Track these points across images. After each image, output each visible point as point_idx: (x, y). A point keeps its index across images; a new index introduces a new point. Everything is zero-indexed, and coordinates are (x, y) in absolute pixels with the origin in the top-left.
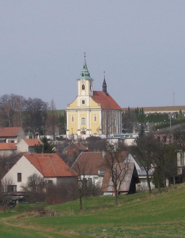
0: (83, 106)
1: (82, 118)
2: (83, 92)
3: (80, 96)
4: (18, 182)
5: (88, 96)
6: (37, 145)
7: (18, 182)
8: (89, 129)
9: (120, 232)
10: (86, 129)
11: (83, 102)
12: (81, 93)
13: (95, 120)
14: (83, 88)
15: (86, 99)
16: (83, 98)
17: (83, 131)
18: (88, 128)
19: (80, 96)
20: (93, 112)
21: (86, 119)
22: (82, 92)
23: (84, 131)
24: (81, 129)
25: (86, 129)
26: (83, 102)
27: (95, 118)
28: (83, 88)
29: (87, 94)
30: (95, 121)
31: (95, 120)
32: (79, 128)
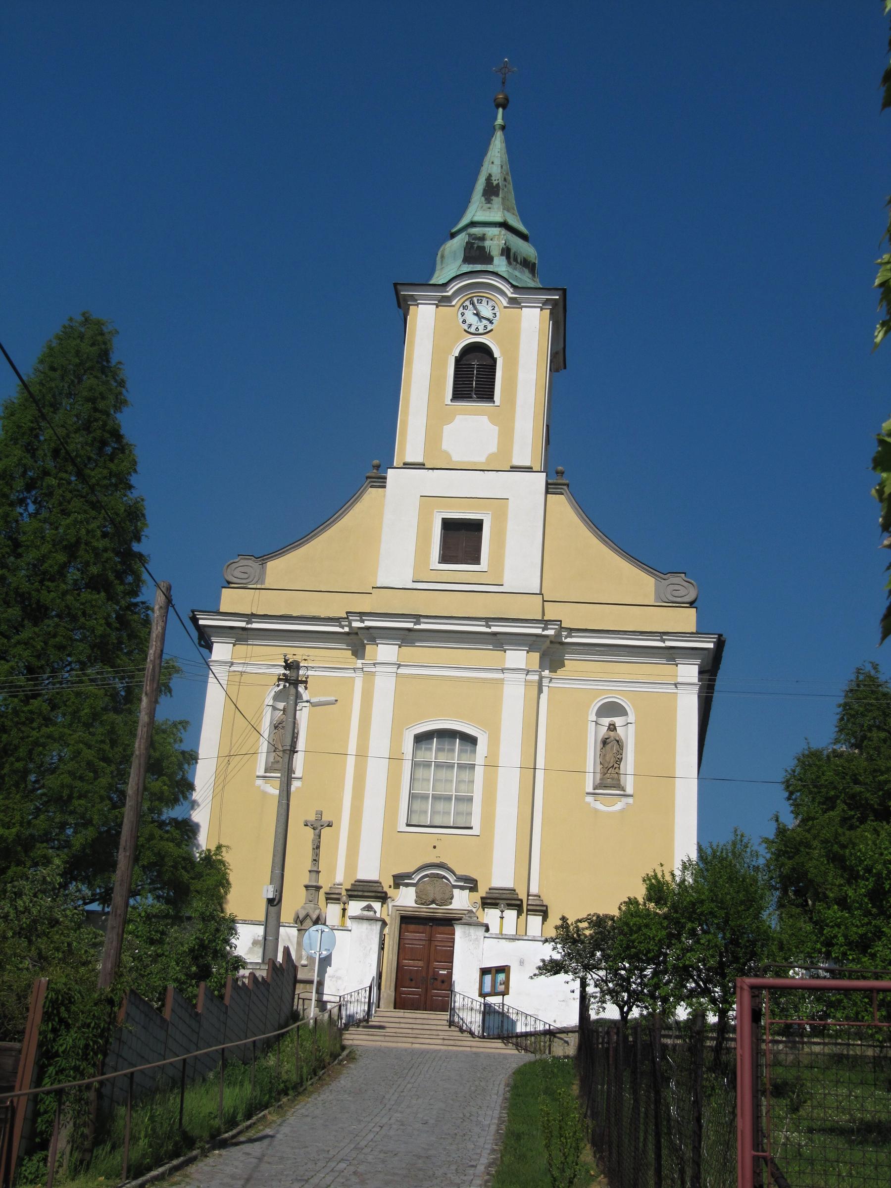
0: (457, 592)
1: (422, 739)
2: (471, 430)
3: (420, 466)
4: (481, 969)
5: (529, 469)
6: (709, 851)
7: (481, 969)
8: (523, 896)
9: (709, 1047)
10: (471, 884)
11: (461, 539)
12: (433, 437)
13: (610, 778)
14: (475, 376)
15: (499, 504)
16: (462, 494)
17: (425, 911)
18: (501, 875)
19: (420, 466)
20: (586, 681)
21: (482, 747)
22: (448, 430)
23: (439, 911)
24: (399, 880)
25: (471, 884)
26: (461, 539)
27: (611, 747)
28: (475, 376)
29: (527, 444)
30: (601, 785)
31: (610, 778)
32: (369, 871)
